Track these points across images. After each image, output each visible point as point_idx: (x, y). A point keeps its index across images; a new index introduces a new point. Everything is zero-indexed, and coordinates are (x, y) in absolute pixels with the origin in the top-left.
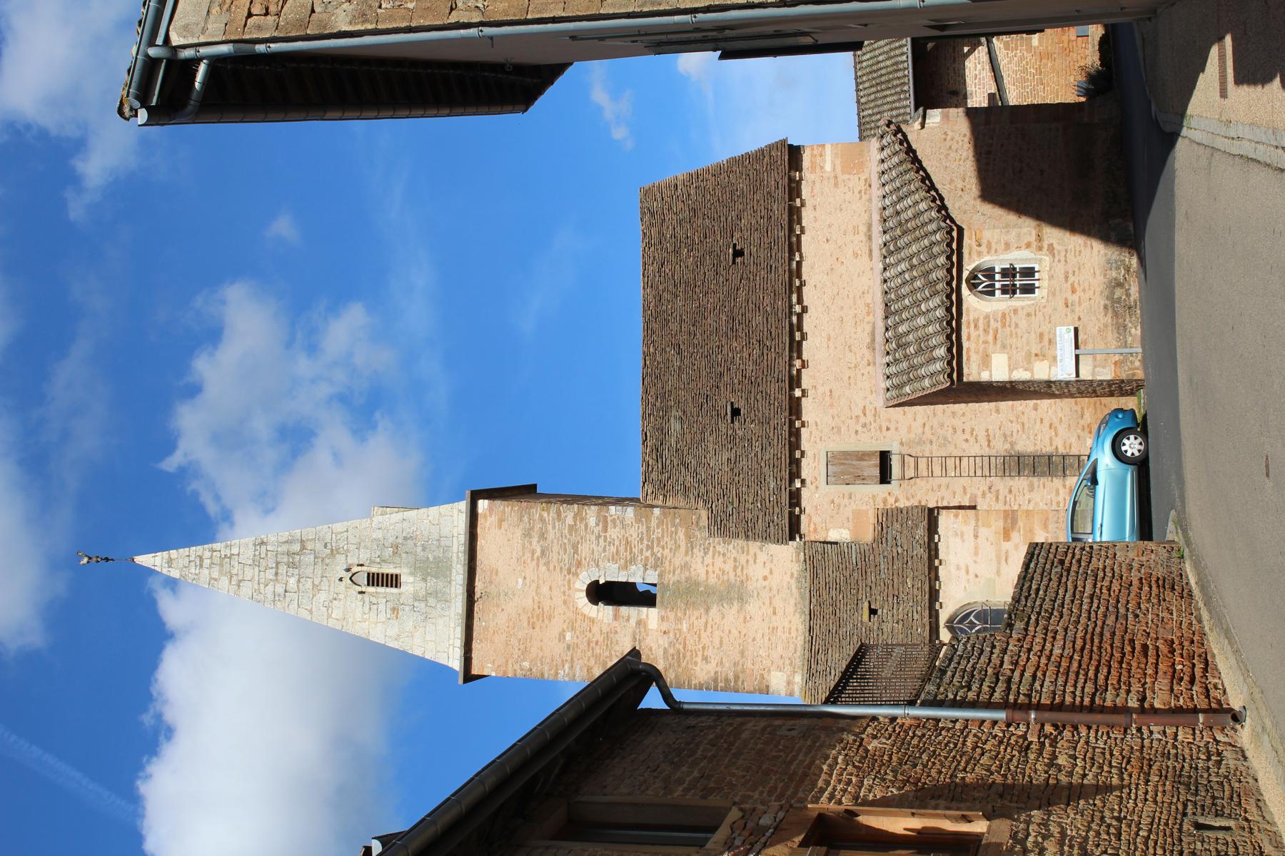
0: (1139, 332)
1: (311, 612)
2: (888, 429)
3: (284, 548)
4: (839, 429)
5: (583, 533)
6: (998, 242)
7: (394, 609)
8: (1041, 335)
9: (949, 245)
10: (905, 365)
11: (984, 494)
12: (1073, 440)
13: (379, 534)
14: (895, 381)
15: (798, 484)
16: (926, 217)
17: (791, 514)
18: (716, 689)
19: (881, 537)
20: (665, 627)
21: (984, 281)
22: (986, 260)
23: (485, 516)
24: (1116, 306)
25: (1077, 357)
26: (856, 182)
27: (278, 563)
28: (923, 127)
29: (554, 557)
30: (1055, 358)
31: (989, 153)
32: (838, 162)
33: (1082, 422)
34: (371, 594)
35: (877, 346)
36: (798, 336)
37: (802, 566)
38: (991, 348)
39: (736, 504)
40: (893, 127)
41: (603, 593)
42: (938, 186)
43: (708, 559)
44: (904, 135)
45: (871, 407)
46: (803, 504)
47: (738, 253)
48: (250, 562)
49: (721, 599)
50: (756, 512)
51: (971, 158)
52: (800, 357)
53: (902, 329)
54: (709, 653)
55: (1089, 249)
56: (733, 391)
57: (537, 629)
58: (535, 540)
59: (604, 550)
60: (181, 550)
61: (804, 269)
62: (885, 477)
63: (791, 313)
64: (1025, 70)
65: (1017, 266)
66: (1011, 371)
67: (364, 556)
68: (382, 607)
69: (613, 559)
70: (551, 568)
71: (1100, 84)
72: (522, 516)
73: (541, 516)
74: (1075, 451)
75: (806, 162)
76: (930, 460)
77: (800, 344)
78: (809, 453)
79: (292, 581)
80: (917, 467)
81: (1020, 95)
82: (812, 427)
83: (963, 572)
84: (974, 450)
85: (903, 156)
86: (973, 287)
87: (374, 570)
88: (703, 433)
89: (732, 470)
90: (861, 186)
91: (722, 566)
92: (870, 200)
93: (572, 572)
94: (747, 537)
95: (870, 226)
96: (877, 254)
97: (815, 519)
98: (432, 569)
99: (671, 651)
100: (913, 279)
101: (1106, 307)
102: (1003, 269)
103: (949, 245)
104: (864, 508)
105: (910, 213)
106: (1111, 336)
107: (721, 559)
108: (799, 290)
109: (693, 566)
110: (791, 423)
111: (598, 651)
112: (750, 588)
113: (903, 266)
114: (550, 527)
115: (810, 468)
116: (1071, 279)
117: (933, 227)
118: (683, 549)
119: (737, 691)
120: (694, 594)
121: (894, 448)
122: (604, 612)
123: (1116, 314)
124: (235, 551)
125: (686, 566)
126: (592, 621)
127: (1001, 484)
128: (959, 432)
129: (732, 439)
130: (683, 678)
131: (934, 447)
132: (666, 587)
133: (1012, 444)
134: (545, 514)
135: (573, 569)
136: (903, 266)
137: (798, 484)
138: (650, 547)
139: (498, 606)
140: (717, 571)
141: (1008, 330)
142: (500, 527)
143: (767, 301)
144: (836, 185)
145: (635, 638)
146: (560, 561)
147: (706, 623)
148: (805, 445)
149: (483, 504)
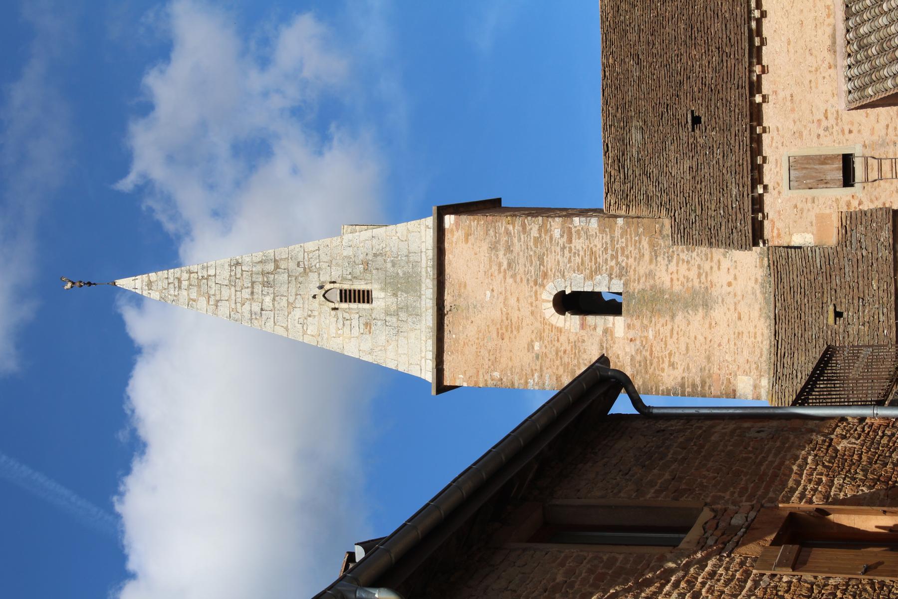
1: (287, 329)
2: (850, 132)
3: (259, 268)
4: (801, 134)
5: (548, 245)
7: (367, 324)
10: (866, 66)
13: (349, 252)
14: (857, 83)
17: (754, 220)
18: (683, 395)
20: (631, 334)
23: (452, 230)
27: (253, 283)
29: (521, 269)
34: (344, 310)
35: (838, 49)
39: (698, 212)
41: (568, 303)
43: (673, 267)
45: (833, 110)
46: (767, 209)
48: (226, 282)
49: (686, 306)
50: (719, 219)
52: (759, 62)
53: (863, 30)
54: (676, 359)
57: (507, 340)
58: (501, 253)
59: (570, 261)
60: (160, 273)
62: (848, 180)
63: (750, 19)
67: (336, 274)
68: (355, 323)
69: (579, 269)
70: (518, 280)
73: (507, 230)
77: (759, 49)
79: (268, 300)
82: (773, 133)
87: (346, 286)
89: (694, 178)
91: (687, 273)
93: (540, 280)
94: (711, 244)
97: (779, 224)
98: (400, 284)
99: (638, 358)
104: (828, 211)
109: (658, 274)
110: (753, 129)
111: (566, 360)
112: (714, 294)
114: (516, 240)
115: (774, 173)
118: (647, 257)
119: (704, 396)
120: (658, 302)
121: (857, 150)
122: (571, 322)
125: (650, 275)
126: (560, 330)
129: (693, 147)
132: (631, 296)
135: (540, 281)
139: (467, 318)
140: (681, 279)
142: (467, 241)
143: (725, 7)
145: (602, 346)
146: (527, 273)
148: (767, 150)
149: (449, 220)
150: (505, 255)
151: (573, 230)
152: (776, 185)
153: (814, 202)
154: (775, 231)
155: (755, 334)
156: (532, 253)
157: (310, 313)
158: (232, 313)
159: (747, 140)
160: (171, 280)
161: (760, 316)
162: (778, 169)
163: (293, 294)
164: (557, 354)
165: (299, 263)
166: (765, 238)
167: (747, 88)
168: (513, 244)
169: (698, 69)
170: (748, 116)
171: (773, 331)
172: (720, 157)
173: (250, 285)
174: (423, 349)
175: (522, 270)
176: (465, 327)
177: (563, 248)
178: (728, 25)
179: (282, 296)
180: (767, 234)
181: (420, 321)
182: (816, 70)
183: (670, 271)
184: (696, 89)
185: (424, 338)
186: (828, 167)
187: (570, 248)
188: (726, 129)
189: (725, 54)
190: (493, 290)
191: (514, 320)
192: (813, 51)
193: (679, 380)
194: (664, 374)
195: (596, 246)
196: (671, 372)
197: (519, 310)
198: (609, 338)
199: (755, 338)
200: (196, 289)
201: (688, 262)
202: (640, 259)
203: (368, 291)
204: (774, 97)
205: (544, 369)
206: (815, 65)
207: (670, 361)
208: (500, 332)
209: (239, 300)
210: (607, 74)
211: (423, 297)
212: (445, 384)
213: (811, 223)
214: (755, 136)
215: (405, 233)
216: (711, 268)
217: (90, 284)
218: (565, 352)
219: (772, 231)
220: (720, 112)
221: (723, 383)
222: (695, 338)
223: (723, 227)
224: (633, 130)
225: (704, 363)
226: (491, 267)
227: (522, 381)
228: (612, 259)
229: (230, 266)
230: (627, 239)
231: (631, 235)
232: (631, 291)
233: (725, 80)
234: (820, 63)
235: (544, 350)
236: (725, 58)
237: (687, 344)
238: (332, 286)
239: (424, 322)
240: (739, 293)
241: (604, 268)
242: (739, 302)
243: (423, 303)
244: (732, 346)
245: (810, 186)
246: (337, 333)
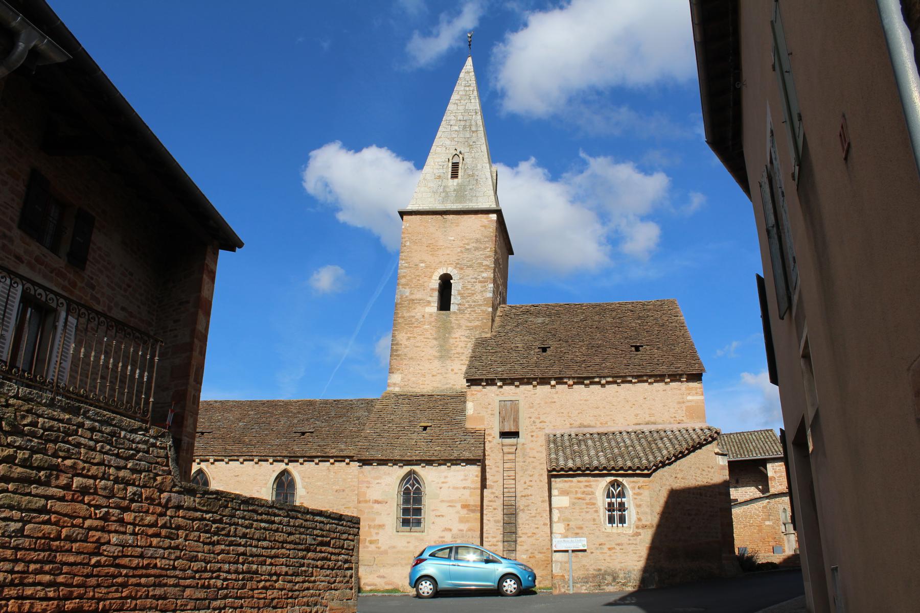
0: (583, 591)
3: (473, 123)
6: (642, 500)
7: (440, 176)
8: (581, 528)
9: (638, 468)
10: (567, 444)
11: (493, 493)
12: (525, 547)
13: (479, 167)
14: (559, 439)
15: (499, 384)
16: (658, 454)
17: (482, 380)
19: (467, 432)
20: (426, 316)
21: (616, 491)
22: (629, 492)
24: (600, 577)
25: (567, 551)
26: (681, 415)
28: (716, 454)
29: (466, 255)
30: (566, 537)
31: (701, 494)
32: (693, 404)
33: (536, 552)
36: (587, 382)
37: (459, 390)
38: (573, 496)
40: (715, 435)
41: (446, 283)
42: (678, 462)
43: (463, 339)
44: (710, 442)
46: (488, 387)
47: (637, 348)
51: (697, 483)
52: (575, 383)
53: (590, 442)
54: (412, 340)
55: (637, 559)
58: (474, 245)
61: (627, 385)
62: (504, 435)
63: (600, 377)
64: (751, 517)
65: (626, 513)
66: (558, 508)
67: (468, 160)
68: (441, 171)
69: (464, 287)
71: (747, 563)
74: (518, 548)
75: (691, 384)
76: (514, 461)
77: (582, 383)
78: (518, 390)
79: (456, 128)
80: (509, 453)
81: (737, 515)
82: (533, 392)
83: (443, 480)
84: (520, 488)
85: (697, 440)
86: (612, 484)
87: (460, 165)
90: (679, 418)
92: (670, 423)
93: (459, 266)
95: (654, 423)
96: (638, 428)
97: (479, 395)
98: (460, 193)
99: (414, 320)
100: (619, 448)
101: (600, 570)
102: (624, 504)
103: (638, 468)
105: (661, 445)
106: (581, 573)
108: (615, 382)
110: (535, 379)
111: (414, 281)
113: (628, 442)
115: (509, 391)
116: (618, 548)
117: (651, 458)
118: (469, 324)
120: (444, 331)
121: (521, 440)
122: (435, 283)
123: (595, 576)
125: (459, 326)
126: (431, 277)
127: (499, 503)
128: (530, 478)
131: (521, 464)
132: (448, 316)
133: (523, 510)
136: (628, 442)
137: (499, 384)
138: (470, 306)
141: (585, 506)
144: (679, 403)
148: (522, 387)
149: (494, 217)
177: (476, 278)
225: (409, 356)
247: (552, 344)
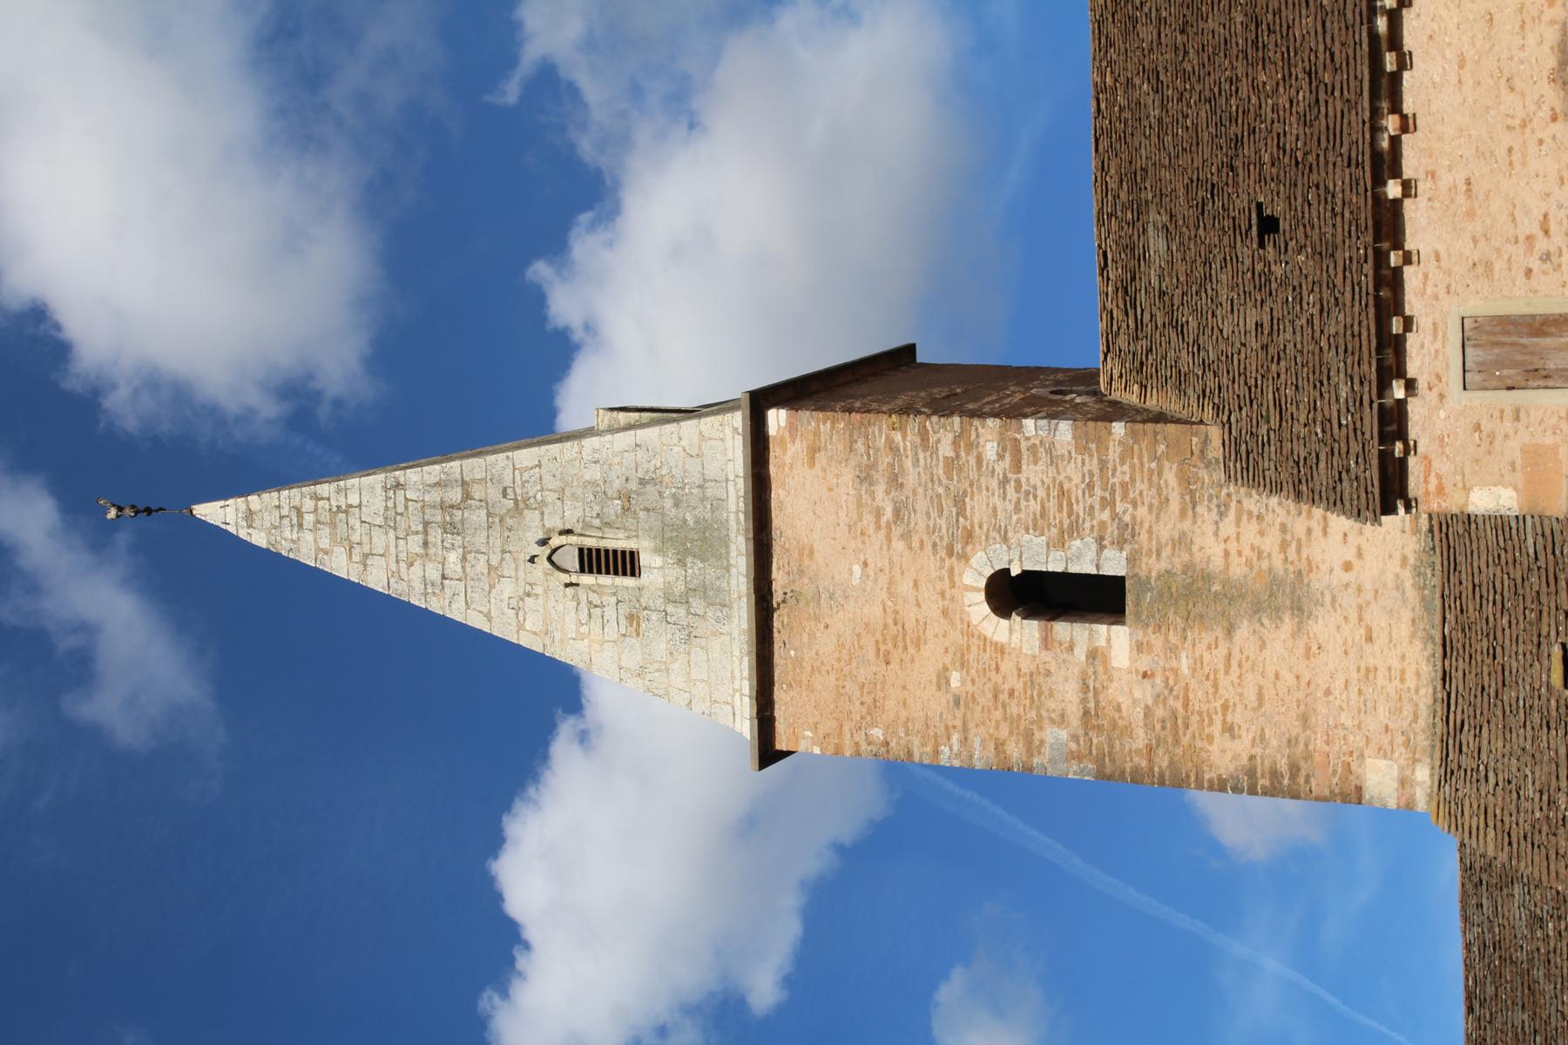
1: (488, 617)
3: (434, 496)
4: (1489, 266)
5: (973, 475)
7: (631, 618)
13: (594, 473)
15: (1399, 392)
17: (1385, 457)
18: (1252, 791)
20: (1145, 663)
27: (426, 524)
29: (919, 521)
34: (590, 588)
36: (1390, 61)
41: (1018, 594)
43: (1228, 527)
46: (1413, 432)
49: (1257, 609)
50: (1314, 446)
52: (1396, 108)
54: (1236, 717)
56: (1261, 179)
57: (895, 665)
58: (880, 489)
59: (1017, 509)
60: (266, 496)
67: (571, 515)
68: (610, 613)
70: (916, 544)
72: (853, 442)
73: (890, 441)
77: (1396, 78)
78: (1423, 320)
79: (453, 557)
87: (590, 542)
88: (1207, 263)
89: (1265, 347)
91: (1258, 541)
93: (958, 546)
94: (1298, 495)
97: (1441, 466)
98: (694, 542)
99: (1160, 712)
104: (1549, 440)
107: (1254, 526)
109: (1198, 541)
110: (1380, 258)
111: (1014, 709)
112: (1315, 585)
114: (908, 463)
115: (1430, 353)
118: (1174, 505)
119: (1296, 796)
120: (1200, 598)
124: (353, 499)
126: (1001, 649)
129: (1263, 281)
130: (1186, 767)
132: (1144, 585)
134: (898, 437)
135: (958, 547)
137: (1399, 392)
139: (817, 619)
140: (1247, 552)
142: (812, 462)
146: (931, 531)
147: (1229, 656)
148: (1413, 303)
149: (777, 419)
150: (887, 492)
151: (1024, 445)
152: (1434, 381)
153: (1517, 418)
154: (1433, 481)
155: (1403, 672)
156: (941, 490)
157: (528, 588)
158: (392, 581)
159: (1368, 282)
160: (285, 512)
161: (1413, 635)
162: (1438, 345)
163: (498, 550)
164: (996, 697)
165: (505, 490)
166: (1411, 495)
167: (1367, 168)
168: (903, 470)
169: (1270, 115)
170: (1371, 230)
171: (1440, 675)
172: (1316, 311)
173: (420, 528)
174: (737, 673)
175: (922, 525)
176: (812, 636)
177: (1004, 482)
178: (1328, 24)
179: (478, 552)
180: (1415, 485)
181: (729, 617)
182: (1524, 125)
183: (1222, 535)
184: (1266, 158)
185: (737, 653)
186: (1548, 341)
187: (1018, 482)
188: (1324, 253)
189: (1322, 87)
190: (865, 564)
191: (910, 625)
192: (1517, 83)
193: (1245, 760)
194: (1214, 749)
195: (1070, 479)
196: (1228, 744)
197: (918, 605)
198: (1100, 669)
199: (1403, 680)
200: (327, 530)
201: (1260, 517)
202: (1160, 509)
203: (632, 553)
204: (1429, 184)
205: (971, 725)
206: (1520, 114)
207: (1224, 721)
208: (882, 648)
209: (403, 556)
210: (1103, 106)
211: (734, 571)
212: (778, 747)
213: (1513, 464)
214: (1385, 272)
215: (696, 440)
216: (1309, 531)
217: (149, 511)
218: (1011, 693)
219: (1426, 481)
220: (1315, 214)
221: (1335, 772)
222: (1277, 676)
223: (1322, 465)
224: (1150, 229)
225: (1296, 729)
226: (860, 518)
227: (928, 749)
228: (1103, 508)
229: (386, 489)
230: (1132, 467)
231: (1141, 457)
232: (1143, 574)
233: (1324, 144)
234: (1532, 108)
235: (969, 687)
236: (1322, 96)
237: (1260, 688)
238: (563, 539)
239: (736, 620)
240: (1368, 586)
241: (1088, 525)
242: (1368, 603)
243: (733, 582)
244: (1354, 696)
245: (1510, 383)
246: (578, 632)
247: (1245, 195)
